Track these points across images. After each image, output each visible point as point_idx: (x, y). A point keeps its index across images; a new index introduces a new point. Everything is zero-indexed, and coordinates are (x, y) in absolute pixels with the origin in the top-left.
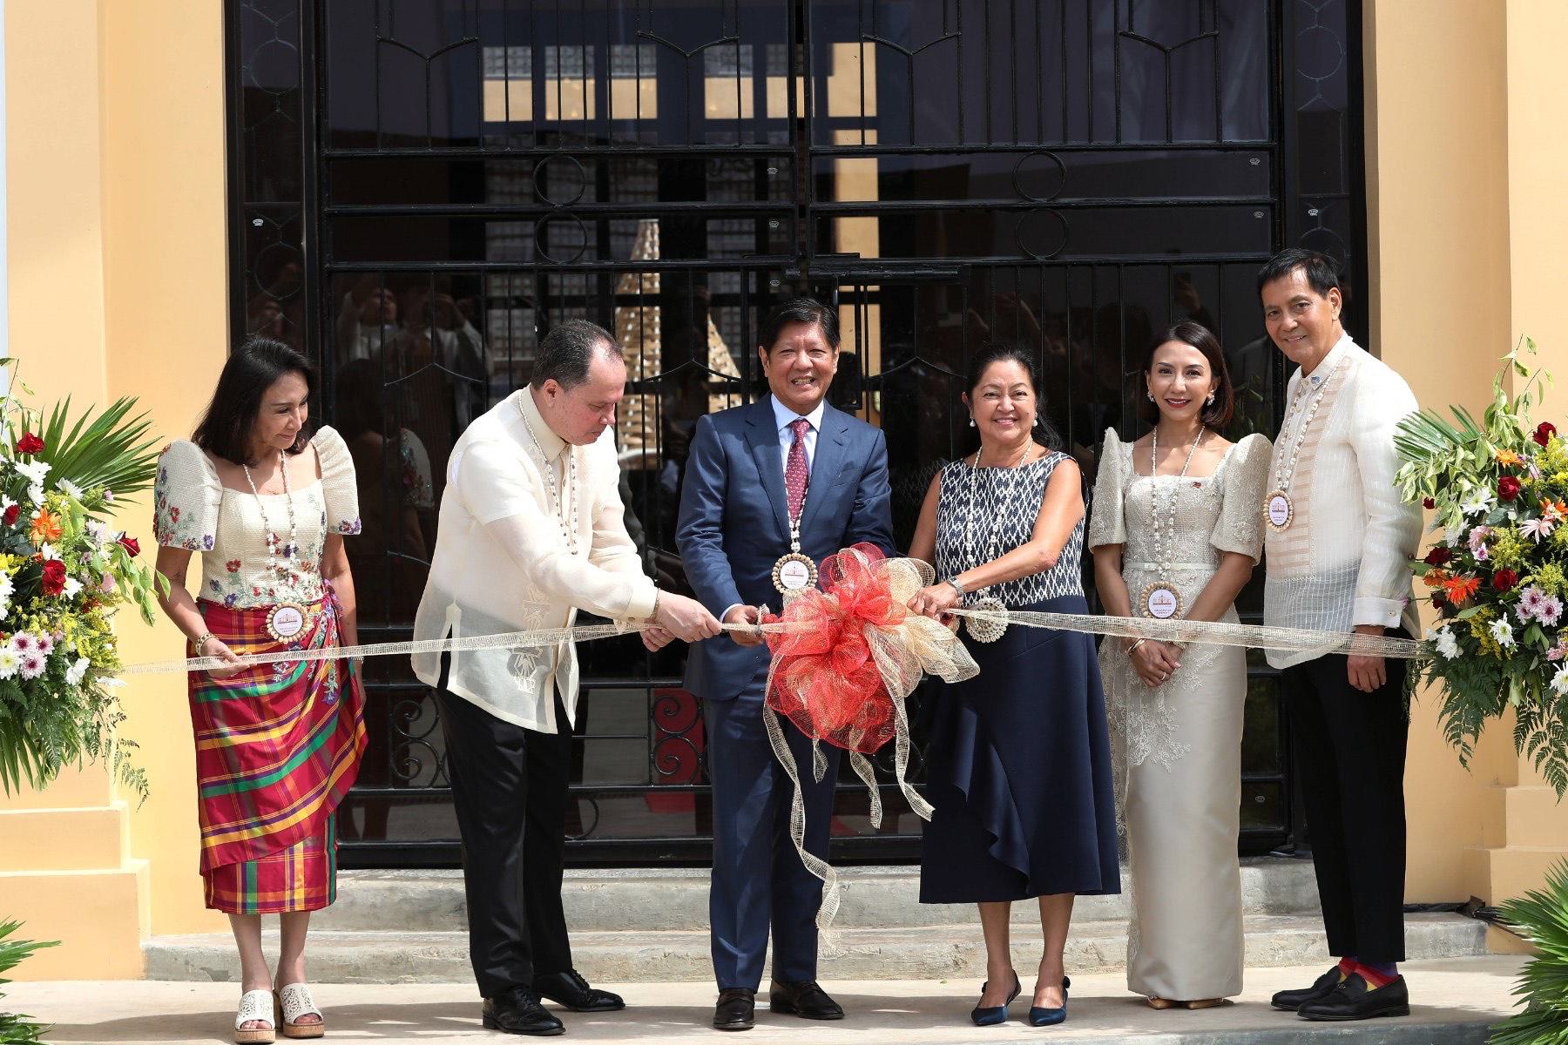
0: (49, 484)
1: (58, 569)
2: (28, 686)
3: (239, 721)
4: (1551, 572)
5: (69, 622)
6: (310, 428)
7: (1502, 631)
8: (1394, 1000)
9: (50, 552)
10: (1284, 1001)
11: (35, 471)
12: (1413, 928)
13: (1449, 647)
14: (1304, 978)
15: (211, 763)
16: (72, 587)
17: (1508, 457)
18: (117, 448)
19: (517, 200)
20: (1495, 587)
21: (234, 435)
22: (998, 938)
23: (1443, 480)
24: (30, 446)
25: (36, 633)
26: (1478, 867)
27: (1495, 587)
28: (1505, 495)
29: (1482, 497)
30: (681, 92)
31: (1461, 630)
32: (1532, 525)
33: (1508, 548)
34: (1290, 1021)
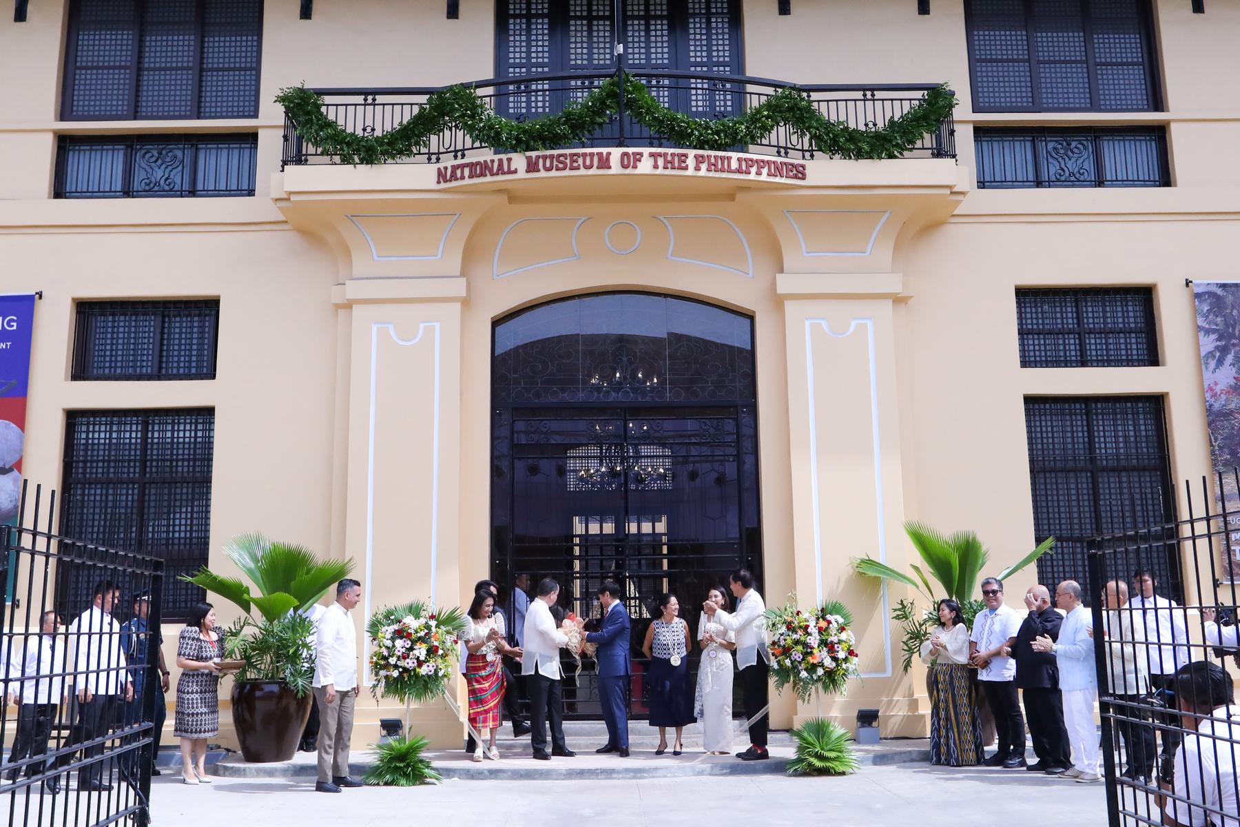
0: (437, 626)
1: (437, 648)
2: (429, 677)
3: (478, 682)
4: (800, 648)
5: (439, 660)
6: (494, 612)
7: (788, 662)
8: (765, 755)
9: (436, 643)
10: (739, 755)
11: (433, 623)
12: (769, 736)
13: (776, 667)
14: (744, 749)
15: (472, 692)
16: (440, 652)
17: (789, 619)
18: (455, 619)
19: (73, 592)
20: (786, 651)
21: (476, 612)
22: (663, 734)
23: (774, 625)
24: (432, 617)
25: (432, 663)
26: (791, 721)
27: (786, 651)
28: (788, 628)
29: (783, 629)
30: (619, 527)
31: (778, 662)
32: (795, 636)
33: (789, 641)
34: (740, 761)
